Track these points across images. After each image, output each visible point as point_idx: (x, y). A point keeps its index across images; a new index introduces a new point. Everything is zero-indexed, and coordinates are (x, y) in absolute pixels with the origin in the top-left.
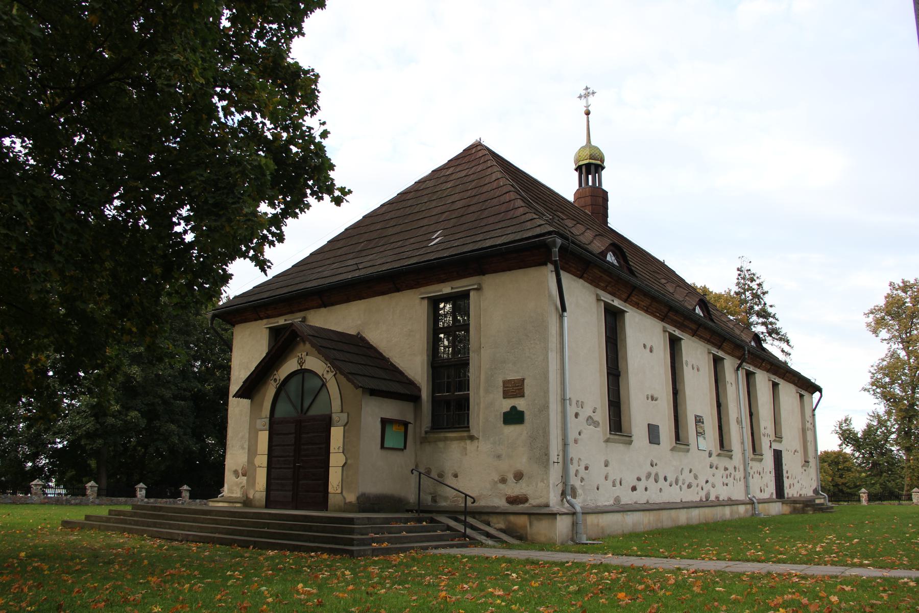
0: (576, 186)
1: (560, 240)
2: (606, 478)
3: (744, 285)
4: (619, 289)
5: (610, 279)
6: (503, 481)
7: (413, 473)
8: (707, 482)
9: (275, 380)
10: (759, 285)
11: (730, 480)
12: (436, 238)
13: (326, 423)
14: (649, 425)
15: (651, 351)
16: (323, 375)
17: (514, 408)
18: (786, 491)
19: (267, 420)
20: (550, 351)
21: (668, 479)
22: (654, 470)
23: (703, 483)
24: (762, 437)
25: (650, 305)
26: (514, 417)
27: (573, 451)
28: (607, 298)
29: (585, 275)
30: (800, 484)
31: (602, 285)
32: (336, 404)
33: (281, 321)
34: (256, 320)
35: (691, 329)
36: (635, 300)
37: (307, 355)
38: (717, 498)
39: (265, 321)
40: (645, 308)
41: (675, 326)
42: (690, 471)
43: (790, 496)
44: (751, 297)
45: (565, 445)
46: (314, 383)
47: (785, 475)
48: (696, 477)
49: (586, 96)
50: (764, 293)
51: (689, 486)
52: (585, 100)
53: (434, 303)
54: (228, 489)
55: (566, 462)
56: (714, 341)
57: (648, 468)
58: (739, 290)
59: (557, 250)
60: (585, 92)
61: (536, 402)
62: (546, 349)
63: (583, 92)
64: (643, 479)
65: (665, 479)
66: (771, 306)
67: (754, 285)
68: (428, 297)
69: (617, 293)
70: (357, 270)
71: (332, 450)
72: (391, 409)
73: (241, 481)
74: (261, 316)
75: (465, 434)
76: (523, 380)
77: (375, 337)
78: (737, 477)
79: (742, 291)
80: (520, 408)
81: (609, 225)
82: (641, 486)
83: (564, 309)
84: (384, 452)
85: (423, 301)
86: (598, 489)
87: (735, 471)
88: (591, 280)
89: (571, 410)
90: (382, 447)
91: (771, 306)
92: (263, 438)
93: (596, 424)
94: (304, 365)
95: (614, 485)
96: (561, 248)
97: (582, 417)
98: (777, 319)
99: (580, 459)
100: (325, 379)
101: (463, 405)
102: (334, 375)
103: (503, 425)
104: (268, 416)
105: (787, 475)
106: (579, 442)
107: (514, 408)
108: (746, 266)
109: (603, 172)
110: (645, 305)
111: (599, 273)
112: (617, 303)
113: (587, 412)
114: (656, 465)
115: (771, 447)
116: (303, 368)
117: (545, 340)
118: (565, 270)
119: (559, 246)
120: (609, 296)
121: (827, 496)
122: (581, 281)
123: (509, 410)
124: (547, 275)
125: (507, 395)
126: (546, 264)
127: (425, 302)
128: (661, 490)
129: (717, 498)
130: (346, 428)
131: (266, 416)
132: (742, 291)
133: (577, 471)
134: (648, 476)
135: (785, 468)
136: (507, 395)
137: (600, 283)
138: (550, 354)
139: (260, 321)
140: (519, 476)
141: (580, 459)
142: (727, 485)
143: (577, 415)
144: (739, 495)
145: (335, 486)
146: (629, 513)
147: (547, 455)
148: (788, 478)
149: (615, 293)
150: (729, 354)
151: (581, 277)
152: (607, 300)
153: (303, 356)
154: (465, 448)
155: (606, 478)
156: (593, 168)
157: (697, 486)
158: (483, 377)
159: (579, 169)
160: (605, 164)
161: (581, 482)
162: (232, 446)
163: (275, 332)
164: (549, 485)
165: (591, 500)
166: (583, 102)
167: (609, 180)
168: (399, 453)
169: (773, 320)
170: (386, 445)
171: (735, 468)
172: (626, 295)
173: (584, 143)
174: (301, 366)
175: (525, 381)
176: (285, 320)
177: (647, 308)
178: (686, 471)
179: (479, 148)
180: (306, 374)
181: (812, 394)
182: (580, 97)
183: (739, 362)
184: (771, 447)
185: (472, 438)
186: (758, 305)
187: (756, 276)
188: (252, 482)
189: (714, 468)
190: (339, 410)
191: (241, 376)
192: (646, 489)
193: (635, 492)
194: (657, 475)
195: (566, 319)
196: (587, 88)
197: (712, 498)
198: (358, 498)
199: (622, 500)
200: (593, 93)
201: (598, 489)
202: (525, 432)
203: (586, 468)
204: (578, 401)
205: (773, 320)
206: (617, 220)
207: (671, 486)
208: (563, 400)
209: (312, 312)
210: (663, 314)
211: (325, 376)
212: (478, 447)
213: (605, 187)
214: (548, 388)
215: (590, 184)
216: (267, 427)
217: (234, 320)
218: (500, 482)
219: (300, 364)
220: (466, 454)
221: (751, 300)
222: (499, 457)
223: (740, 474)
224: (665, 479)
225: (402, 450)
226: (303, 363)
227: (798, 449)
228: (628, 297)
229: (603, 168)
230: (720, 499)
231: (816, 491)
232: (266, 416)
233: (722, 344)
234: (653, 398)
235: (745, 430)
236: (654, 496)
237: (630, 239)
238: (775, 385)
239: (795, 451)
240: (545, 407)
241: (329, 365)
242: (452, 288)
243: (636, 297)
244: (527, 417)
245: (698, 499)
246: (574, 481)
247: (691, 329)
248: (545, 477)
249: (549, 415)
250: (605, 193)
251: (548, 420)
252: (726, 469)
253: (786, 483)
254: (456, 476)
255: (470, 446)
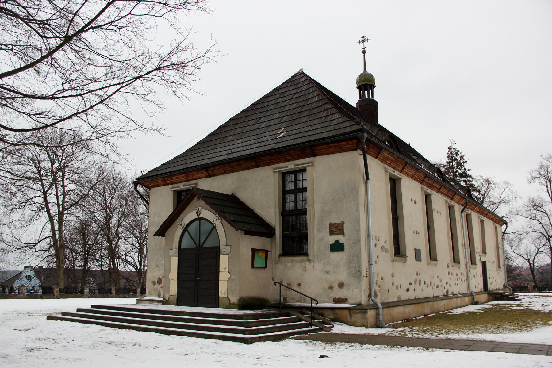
0: (358, 99)
1: (366, 135)
2: (393, 284)
3: (452, 157)
4: (398, 165)
5: (393, 159)
6: (331, 288)
7: (275, 285)
8: (447, 283)
9: (181, 225)
10: (462, 157)
11: (459, 282)
12: (281, 133)
13: (216, 252)
14: (415, 249)
15: (415, 203)
16: (213, 221)
17: (337, 242)
18: (489, 287)
19: (177, 250)
20: (360, 205)
21: (426, 282)
22: (418, 278)
23: (444, 284)
24: (476, 254)
25: (415, 174)
26: (337, 247)
27: (375, 269)
28: (390, 170)
29: (379, 156)
30: (496, 282)
31: (388, 162)
32: (223, 241)
33: (181, 186)
34: (164, 185)
35: (437, 188)
36: (406, 171)
37: (202, 209)
38: (453, 293)
39: (170, 186)
40: (412, 176)
41: (428, 187)
42: (438, 277)
43: (491, 289)
44: (456, 165)
45: (370, 265)
46: (206, 227)
47: (488, 276)
48: (441, 281)
49: (363, 41)
50: (464, 162)
51: (437, 287)
52: (362, 44)
53: (284, 175)
54: (149, 293)
55: (370, 275)
56: (449, 195)
57: (415, 277)
58: (449, 160)
59: (365, 141)
60: (362, 39)
61: (352, 238)
62: (358, 205)
63: (361, 39)
64: (413, 283)
65: (425, 283)
66: (469, 170)
67: (458, 158)
68: (278, 171)
69: (396, 167)
70: (230, 153)
71: (220, 270)
72: (257, 242)
73: (157, 287)
74: (168, 183)
75: (305, 258)
76: (343, 223)
77: (243, 196)
78: (463, 280)
79: (451, 161)
80: (341, 242)
81: (378, 123)
82: (411, 288)
83: (368, 178)
84: (254, 271)
85: (275, 173)
86: (388, 291)
87: (462, 276)
88: (382, 159)
89: (373, 243)
90: (253, 266)
91: (469, 170)
92: (174, 262)
93: (386, 251)
94: (200, 215)
95: (397, 289)
96: (367, 140)
97: (379, 247)
98: (472, 178)
99: (378, 273)
100: (215, 224)
101: (303, 238)
102: (221, 222)
103: (330, 252)
104: (177, 248)
105: (489, 277)
106: (378, 262)
107: (337, 242)
108: (453, 146)
109: (375, 90)
110: (412, 174)
111: (387, 155)
112: (396, 173)
113: (381, 243)
114: (419, 274)
115: (480, 259)
116: (200, 217)
117: (357, 199)
118: (369, 155)
119: (365, 139)
120: (391, 169)
121: (511, 289)
122: (376, 160)
123: (334, 243)
124: (357, 156)
125: (332, 233)
126: (356, 149)
127: (277, 174)
128: (422, 290)
129: (453, 293)
130: (230, 255)
131: (176, 247)
132: (451, 161)
133: (377, 281)
134: (416, 281)
135: (488, 272)
136: (332, 233)
137: (387, 161)
138: (360, 207)
139: (167, 186)
140: (341, 285)
141: (378, 273)
142: (457, 285)
143: (376, 246)
144: (464, 290)
145: (223, 292)
146: (407, 306)
147: (360, 271)
148: (490, 278)
149: (395, 167)
150: (457, 203)
151: (376, 158)
152: (391, 172)
153: (199, 209)
154: (305, 267)
155: (393, 284)
156: (362, 87)
157: (442, 286)
158: (316, 221)
159: (359, 87)
160: (376, 84)
161: (379, 287)
162: (151, 265)
163: (178, 194)
164: (361, 291)
165: (385, 299)
166: (361, 45)
167: (378, 94)
168: (263, 270)
169: (471, 179)
170: (255, 266)
171: (462, 274)
172: (402, 168)
173: (362, 71)
174: (199, 216)
175: (344, 224)
176: (184, 186)
177: (413, 176)
178: (436, 277)
179: (302, 75)
180: (202, 221)
181: (502, 226)
182: (359, 42)
183: (463, 207)
184: (480, 259)
185: (309, 260)
186: (460, 169)
187: (460, 152)
188: (167, 288)
189: (450, 274)
190: (225, 244)
191: (155, 221)
192: (414, 290)
193: (408, 292)
194: (420, 280)
195: (369, 185)
196: (363, 37)
197: (450, 293)
198: (239, 300)
199: (402, 298)
200: (368, 40)
201: (388, 291)
202: (345, 257)
203: (382, 279)
204: (376, 237)
205: (471, 179)
206: (383, 120)
207: (427, 287)
208: (369, 236)
209: (201, 180)
210: (422, 179)
211: (215, 222)
212: (314, 266)
213: (376, 98)
214: (360, 229)
215: (366, 96)
216: (177, 254)
217: (150, 185)
218: (329, 289)
219: (197, 214)
220: (306, 271)
221: (456, 166)
222: (328, 272)
223: (464, 278)
224: (425, 283)
225: (264, 268)
226: (199, 214)
227: (495, 261)
228: (403, 169)
229: (374, 87)
230: (454, 294)
231: (505, 286)
232: (176, 247)
233: (453, 197)
234: (416, 232)
235: (466, 249)
236: (420, 294)
237: (393, 133)
238: (482, 222)
239: (493, 262)
240: (358, 241)
241: (217, 215)
242: (295, 165)
243: (407, 169)
244: (346, 247)
245: (442, 295)
246: (375, 287)
247: (437, 188)
248: (359, 286)
249: (360, 246)
250: (376, 103)
251: (360, 249)
252: (457, 275)
253: (489, 281)
254: (299, 285)
255: (308, 265)
